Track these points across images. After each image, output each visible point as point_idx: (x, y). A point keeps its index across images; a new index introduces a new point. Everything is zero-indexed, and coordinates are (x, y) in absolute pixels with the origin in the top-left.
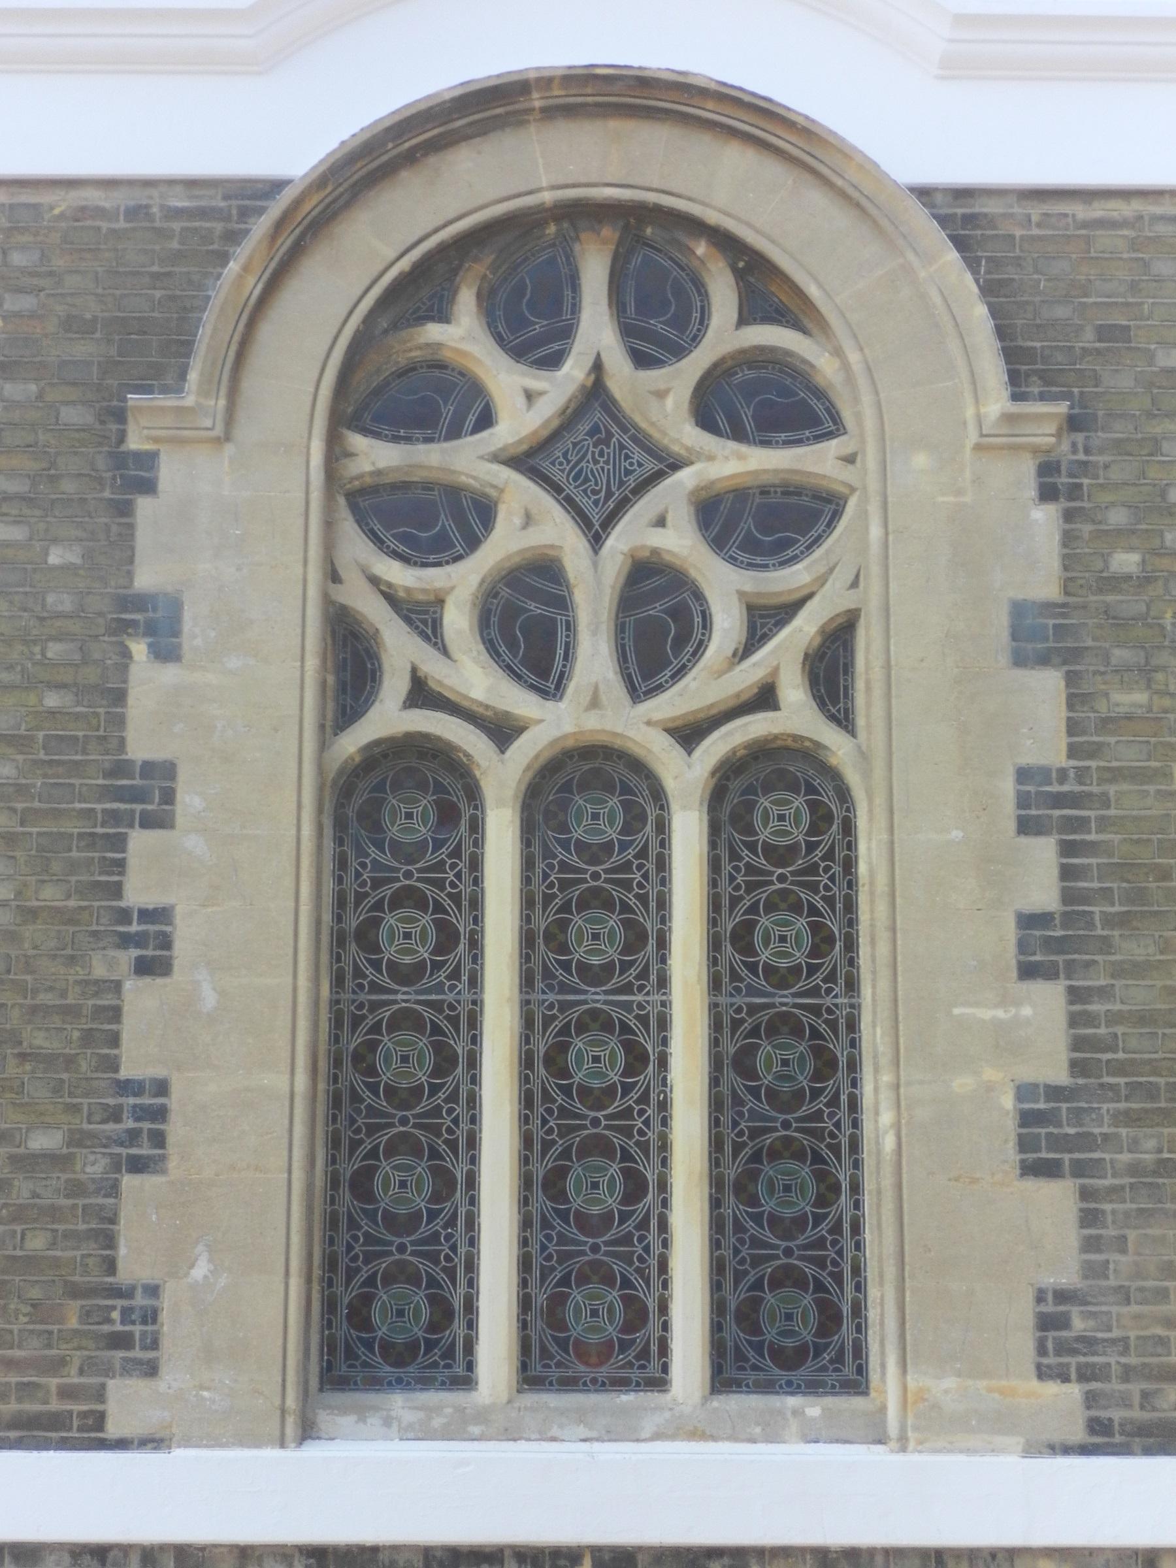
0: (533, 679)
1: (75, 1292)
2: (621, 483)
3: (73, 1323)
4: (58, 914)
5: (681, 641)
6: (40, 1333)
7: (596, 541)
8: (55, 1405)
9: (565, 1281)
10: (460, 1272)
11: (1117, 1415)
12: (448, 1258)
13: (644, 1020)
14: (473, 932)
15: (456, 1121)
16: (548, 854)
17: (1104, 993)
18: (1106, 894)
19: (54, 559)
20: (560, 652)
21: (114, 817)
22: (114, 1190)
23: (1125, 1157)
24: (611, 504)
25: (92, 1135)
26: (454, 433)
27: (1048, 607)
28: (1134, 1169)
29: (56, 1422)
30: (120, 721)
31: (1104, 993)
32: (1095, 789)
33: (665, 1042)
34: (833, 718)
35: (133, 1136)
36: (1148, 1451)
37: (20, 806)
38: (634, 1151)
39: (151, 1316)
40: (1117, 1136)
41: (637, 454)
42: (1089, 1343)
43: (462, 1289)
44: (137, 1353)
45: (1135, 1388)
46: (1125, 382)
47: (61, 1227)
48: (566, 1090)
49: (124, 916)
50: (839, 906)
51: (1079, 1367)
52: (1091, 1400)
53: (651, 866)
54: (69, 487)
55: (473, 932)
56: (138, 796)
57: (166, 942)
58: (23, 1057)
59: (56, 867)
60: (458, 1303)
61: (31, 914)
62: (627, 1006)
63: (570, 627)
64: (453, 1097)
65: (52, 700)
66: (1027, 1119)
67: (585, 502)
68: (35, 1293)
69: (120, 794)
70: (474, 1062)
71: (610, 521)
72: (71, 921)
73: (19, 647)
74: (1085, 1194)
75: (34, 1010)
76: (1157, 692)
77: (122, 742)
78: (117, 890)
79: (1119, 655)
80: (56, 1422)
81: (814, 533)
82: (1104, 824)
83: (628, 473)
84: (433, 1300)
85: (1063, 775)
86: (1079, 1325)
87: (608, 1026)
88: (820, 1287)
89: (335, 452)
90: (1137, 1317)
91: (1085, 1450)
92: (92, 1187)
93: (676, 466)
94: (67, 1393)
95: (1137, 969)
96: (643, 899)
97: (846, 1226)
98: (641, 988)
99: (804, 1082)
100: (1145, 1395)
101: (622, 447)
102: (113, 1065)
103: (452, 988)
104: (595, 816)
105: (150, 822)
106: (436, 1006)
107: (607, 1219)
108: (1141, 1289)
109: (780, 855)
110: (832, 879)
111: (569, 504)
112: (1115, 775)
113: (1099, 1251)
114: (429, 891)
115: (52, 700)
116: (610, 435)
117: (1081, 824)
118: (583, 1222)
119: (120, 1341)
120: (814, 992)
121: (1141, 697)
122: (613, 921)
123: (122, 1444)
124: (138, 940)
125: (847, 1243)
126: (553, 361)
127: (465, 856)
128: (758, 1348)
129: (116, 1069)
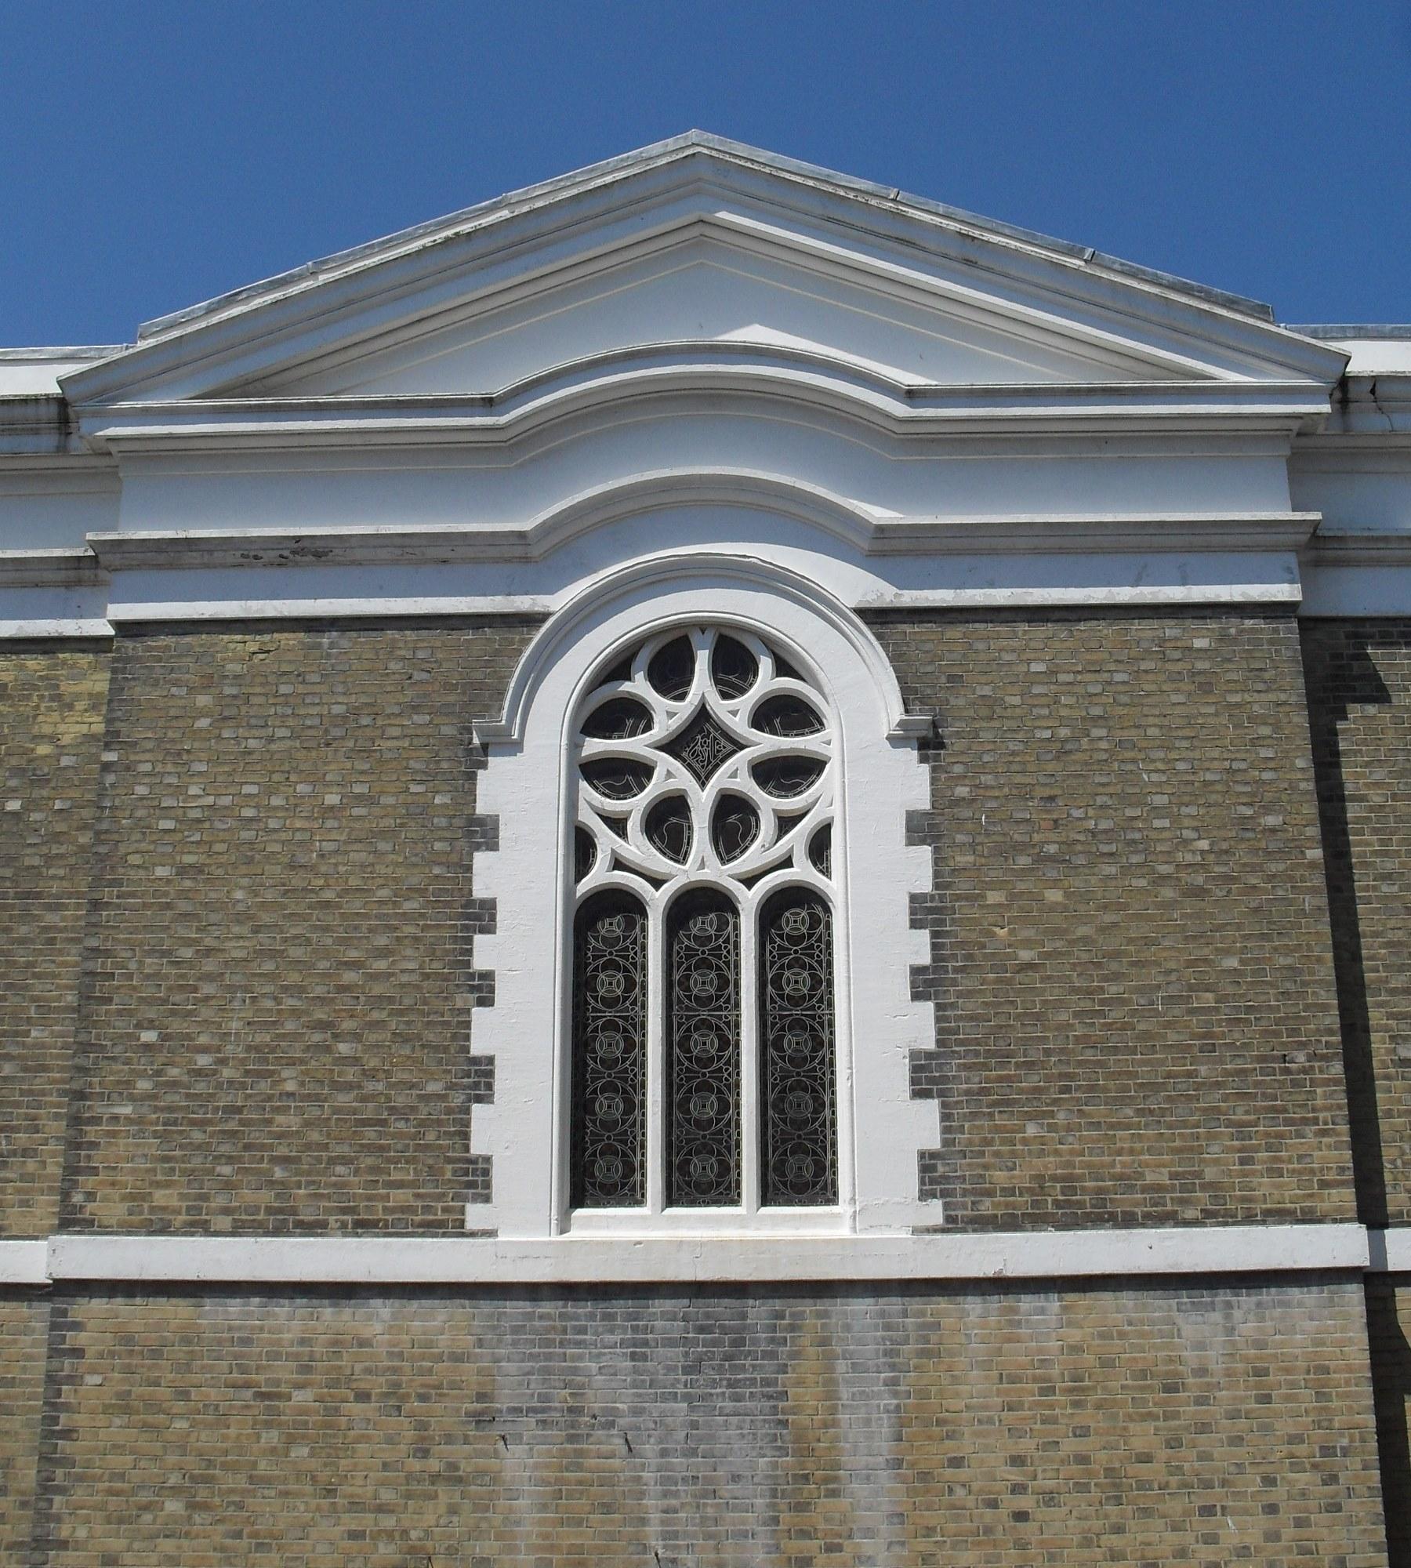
0: (672, 855)
1: (449, 1160)
2: (715, 757)
3: (448, 1175)
4: (439, 976)
5: (744, 837)
6: (433, 1181)
7: (703, 785)
8: (440, 1216)
9: (689, 1153)
10: (638, 1149)
11: (959, 1213)
12: (632, 1142)
13: (728, 1024)
14: (643, 982)
15: (635, 1075)
16: (773, 941)
17: (954, 1006)
18: (954, 957)
19: (437, 801)
20: (685, 841)
21: (466, 928)
22: (468, 1111)
23: (965, 1086)
24: (710, 767)
25: (456, 1084)
26: (633, 734)
27: (925, 814)
28: (968, 1092)
29: (441, 1224)
30: (470, 880)
31: (954, 1006)
32: (949, 905)
33: (738, 1034)
34: (821, 871)
35: (476, 1085)
36: (975, 1231)
37: (421, 923)
38: (724, 1088)
39: (486, 1172)
40: (960, 1076)
41: (723, 742)
42: (945, 1178)
43: (639, 1157)
44: (479, 1191)
45: (968, 1200)
46: (961, 702)
47: (442, 1129)
48: (690, 1059)
49: (472, 976)
50: (824, 965)
51: (941, 1190)
52: (946, 1206)
53: (731, 947)
54: (445, 765)
55: (643, 982)
56: (478, 917)
57: (492, 990)
58: (423, 1046)
59: (438, 953)
60: (637, 1165)
61: (427, 976)
62: (719, 1017)
63: (690, 828)
64: (634, 1064)
65: (437, 871)
66: (915, 1069)
67: (697, 766)
68: (430, 1162)
69: (468, 917)
70: (643, 1046)
71: (708, 777)
72: (445, 980)
73: (421, 845)
74: (944, 1105)
75: (429, 1023)
76: (979, 856)
77: (471, 891)
78: (468, 964)
79: (960, 838)
80: (441, 1224)
81: (811, 780)
82: (954, 921)
83: (718, 751)
84: (624, 1163)
85: (932, 897)
86: (941, 1169)
87: (710, 1027)
88: (815, 1153)
89: (574, 746)
90: (969, 1165)
91: (944, 1231)
92: (457, 1110)
93: (742, 747)
94: (445, 1210)
95: (968, 994)
96: (727, 963)
97: (828, 1123)
98: (726, 1008)
99: (807, 1052)
100: (973, 1203)
101: (715, 739)
102: (467, 1050)
103: (633, 1009)
104: (795, 922)
105: (484, 930)
106: (625, 1018)
107: (710, 1121)
108: (971, 1151)
109: (795, 940)
110: (821, 951)
111: (690, 767)
112: (958, 898)
113: (950, 1133)
114: (621, 962)
115: (437, 871)
116: (709, 733)
117: (942, 922)
118: (698, 1124)
119: (471, 1185)
120: (813, 1008)
121: (971, 859)
122: (713, 975)
123: (473, 1234)
124: (478, 988)
125: (829, 1132)
126: (681, 697)
127: (639, 943)
128: (785, 1184)
129: (469, 1053)
